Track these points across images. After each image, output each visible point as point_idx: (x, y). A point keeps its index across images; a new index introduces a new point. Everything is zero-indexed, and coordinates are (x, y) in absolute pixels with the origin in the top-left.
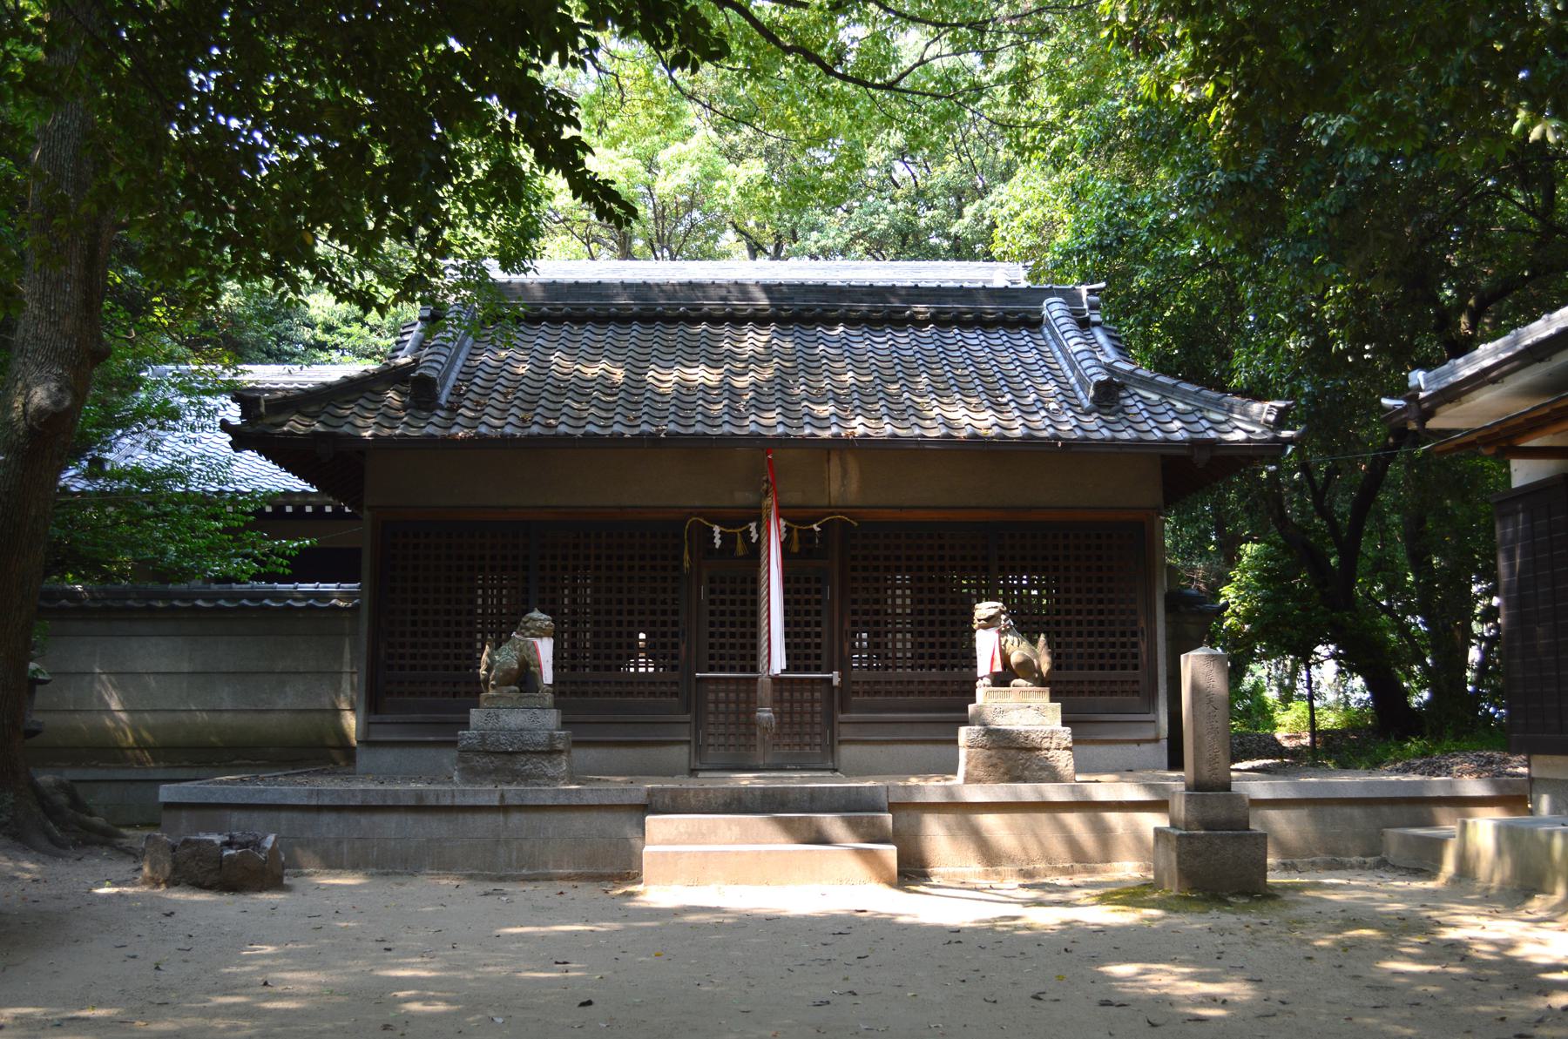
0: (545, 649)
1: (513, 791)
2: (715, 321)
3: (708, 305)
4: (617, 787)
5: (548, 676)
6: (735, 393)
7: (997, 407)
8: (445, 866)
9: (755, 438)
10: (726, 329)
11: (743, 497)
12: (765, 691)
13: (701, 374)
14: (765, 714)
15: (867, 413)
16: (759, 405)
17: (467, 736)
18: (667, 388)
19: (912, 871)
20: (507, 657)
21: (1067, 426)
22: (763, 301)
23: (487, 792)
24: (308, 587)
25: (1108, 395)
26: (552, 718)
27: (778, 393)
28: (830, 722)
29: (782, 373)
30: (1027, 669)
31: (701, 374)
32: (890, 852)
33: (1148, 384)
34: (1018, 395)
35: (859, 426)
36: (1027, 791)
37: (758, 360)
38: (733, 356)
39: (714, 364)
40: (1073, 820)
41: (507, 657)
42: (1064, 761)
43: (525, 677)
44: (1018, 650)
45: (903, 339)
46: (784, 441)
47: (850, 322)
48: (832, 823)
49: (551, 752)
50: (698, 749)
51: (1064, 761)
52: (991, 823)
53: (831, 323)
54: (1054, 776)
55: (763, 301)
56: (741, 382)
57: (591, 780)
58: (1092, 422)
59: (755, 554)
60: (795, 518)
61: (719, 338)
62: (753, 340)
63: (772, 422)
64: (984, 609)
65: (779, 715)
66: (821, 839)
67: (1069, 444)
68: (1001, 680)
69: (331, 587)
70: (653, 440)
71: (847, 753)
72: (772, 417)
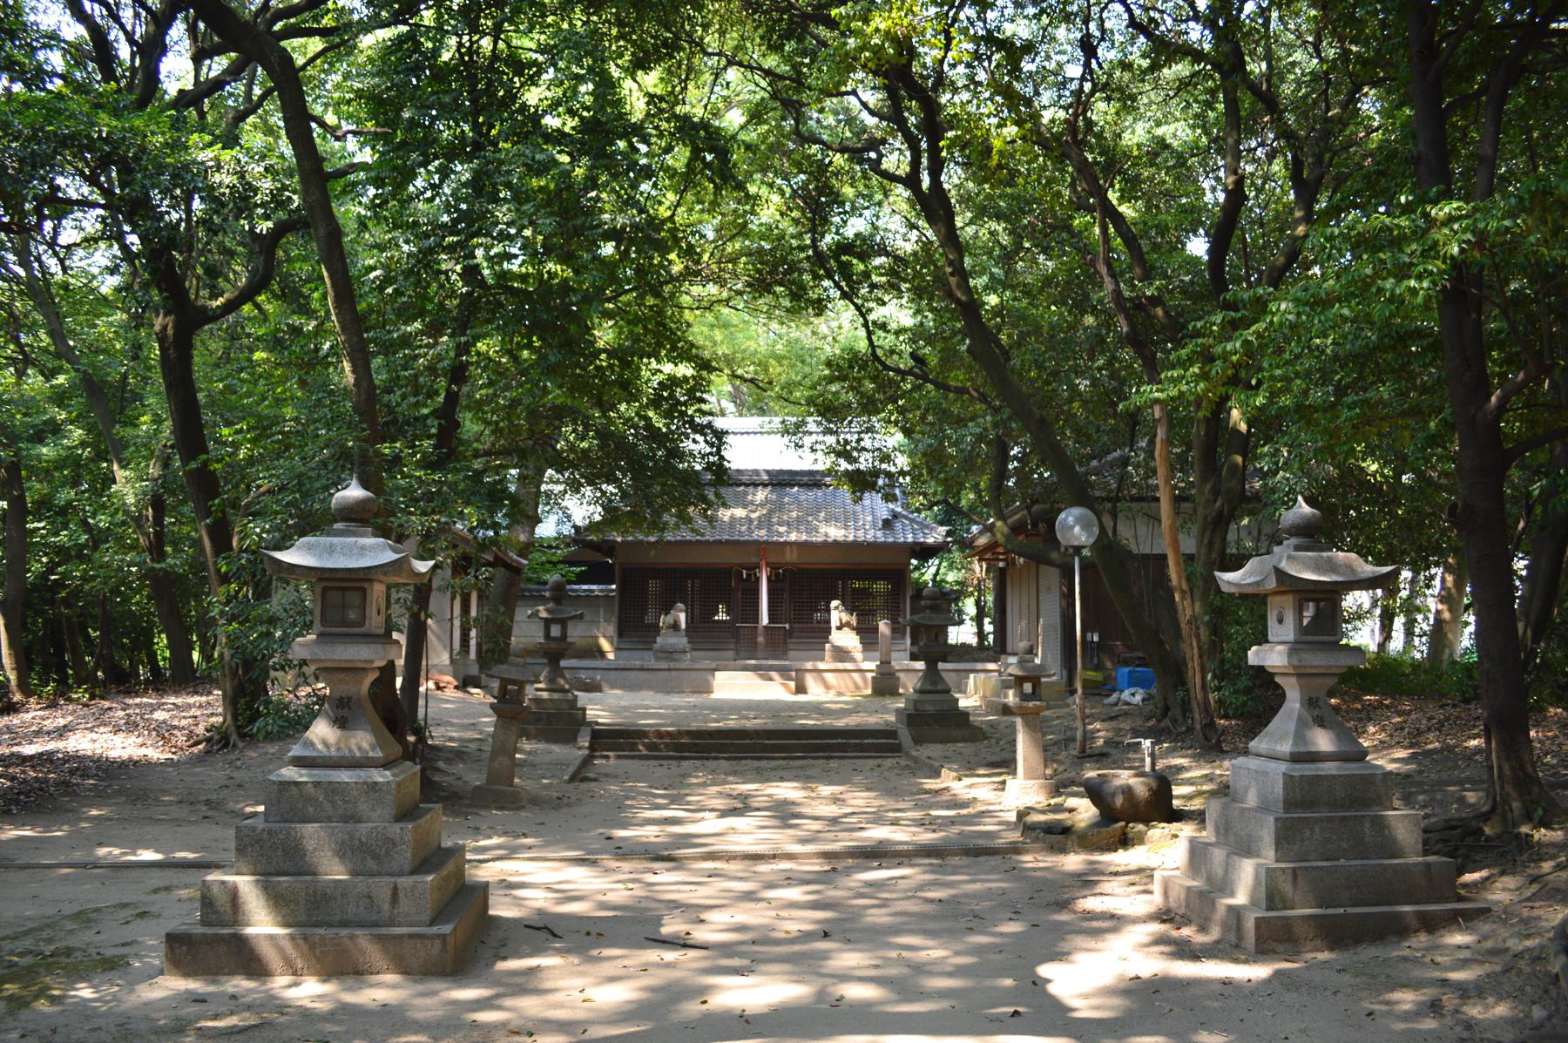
0: (682, 616)
1: (672, 665)
2: (747, 485)
3: (744, 478)
4: (707, 664)
5: (683, 626)
6: (751, 521)
7: (846, 527)
8: (650, 688)
9: (756, 542)
10: (751, 489)
11: (754, 560)
12: (760, 630)
13: (740, 512)
14: (761, 639)
15: (798, 530)
16: (759, 527)
17: (656, 646)
18: (726, 519)
19: (801, 689)
20: (670, 619)
21: (870, 537)
22: (766, 477)
23: (664, 665)
24: (585, 587)
25: (887, 524)
26: (685, 640)
27: (765, 522)
28: (785, 642)
29: (771, 512)
30: (848, 624)
31: (740, 512)
32: (792, 684)
33: (905, 517)
34: (856, 520)
35: (793, 537)
36: (840, 666)
37: (762, 505)
38: (752, 503)
39: (745, 506)
40: (856, 676)
41: (670, 619)
42: (858, 656)
43: (675, 626)
44: (845, 617)
45: (820, 493)
46: (767, 542)
47: (800, 485)
48: (774, 674)
49: (684, 652)
50: (737, 652)
51: (858, 656)
52: (828, 676)
53: (792, 486)
54: (853, 660)
55: (766, 477)
56: (754, 516)
57: (666, 708)
58: (879, 534)
59: (758, 580)
60: (773, 567)
61: (746, 494)
62: (761, 495)
63: (761, 535)
64: (834, 603)
65: (767, 640)
66: (771, 679)
67: (869, 544)
68: (839, 628)
69: (594, 587)
70: (720, 542)
71: (791, 654)
72: (763, 532)
